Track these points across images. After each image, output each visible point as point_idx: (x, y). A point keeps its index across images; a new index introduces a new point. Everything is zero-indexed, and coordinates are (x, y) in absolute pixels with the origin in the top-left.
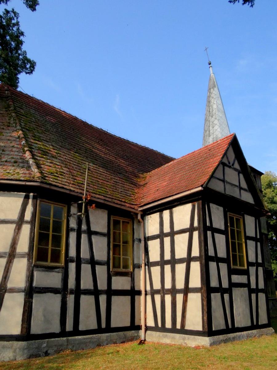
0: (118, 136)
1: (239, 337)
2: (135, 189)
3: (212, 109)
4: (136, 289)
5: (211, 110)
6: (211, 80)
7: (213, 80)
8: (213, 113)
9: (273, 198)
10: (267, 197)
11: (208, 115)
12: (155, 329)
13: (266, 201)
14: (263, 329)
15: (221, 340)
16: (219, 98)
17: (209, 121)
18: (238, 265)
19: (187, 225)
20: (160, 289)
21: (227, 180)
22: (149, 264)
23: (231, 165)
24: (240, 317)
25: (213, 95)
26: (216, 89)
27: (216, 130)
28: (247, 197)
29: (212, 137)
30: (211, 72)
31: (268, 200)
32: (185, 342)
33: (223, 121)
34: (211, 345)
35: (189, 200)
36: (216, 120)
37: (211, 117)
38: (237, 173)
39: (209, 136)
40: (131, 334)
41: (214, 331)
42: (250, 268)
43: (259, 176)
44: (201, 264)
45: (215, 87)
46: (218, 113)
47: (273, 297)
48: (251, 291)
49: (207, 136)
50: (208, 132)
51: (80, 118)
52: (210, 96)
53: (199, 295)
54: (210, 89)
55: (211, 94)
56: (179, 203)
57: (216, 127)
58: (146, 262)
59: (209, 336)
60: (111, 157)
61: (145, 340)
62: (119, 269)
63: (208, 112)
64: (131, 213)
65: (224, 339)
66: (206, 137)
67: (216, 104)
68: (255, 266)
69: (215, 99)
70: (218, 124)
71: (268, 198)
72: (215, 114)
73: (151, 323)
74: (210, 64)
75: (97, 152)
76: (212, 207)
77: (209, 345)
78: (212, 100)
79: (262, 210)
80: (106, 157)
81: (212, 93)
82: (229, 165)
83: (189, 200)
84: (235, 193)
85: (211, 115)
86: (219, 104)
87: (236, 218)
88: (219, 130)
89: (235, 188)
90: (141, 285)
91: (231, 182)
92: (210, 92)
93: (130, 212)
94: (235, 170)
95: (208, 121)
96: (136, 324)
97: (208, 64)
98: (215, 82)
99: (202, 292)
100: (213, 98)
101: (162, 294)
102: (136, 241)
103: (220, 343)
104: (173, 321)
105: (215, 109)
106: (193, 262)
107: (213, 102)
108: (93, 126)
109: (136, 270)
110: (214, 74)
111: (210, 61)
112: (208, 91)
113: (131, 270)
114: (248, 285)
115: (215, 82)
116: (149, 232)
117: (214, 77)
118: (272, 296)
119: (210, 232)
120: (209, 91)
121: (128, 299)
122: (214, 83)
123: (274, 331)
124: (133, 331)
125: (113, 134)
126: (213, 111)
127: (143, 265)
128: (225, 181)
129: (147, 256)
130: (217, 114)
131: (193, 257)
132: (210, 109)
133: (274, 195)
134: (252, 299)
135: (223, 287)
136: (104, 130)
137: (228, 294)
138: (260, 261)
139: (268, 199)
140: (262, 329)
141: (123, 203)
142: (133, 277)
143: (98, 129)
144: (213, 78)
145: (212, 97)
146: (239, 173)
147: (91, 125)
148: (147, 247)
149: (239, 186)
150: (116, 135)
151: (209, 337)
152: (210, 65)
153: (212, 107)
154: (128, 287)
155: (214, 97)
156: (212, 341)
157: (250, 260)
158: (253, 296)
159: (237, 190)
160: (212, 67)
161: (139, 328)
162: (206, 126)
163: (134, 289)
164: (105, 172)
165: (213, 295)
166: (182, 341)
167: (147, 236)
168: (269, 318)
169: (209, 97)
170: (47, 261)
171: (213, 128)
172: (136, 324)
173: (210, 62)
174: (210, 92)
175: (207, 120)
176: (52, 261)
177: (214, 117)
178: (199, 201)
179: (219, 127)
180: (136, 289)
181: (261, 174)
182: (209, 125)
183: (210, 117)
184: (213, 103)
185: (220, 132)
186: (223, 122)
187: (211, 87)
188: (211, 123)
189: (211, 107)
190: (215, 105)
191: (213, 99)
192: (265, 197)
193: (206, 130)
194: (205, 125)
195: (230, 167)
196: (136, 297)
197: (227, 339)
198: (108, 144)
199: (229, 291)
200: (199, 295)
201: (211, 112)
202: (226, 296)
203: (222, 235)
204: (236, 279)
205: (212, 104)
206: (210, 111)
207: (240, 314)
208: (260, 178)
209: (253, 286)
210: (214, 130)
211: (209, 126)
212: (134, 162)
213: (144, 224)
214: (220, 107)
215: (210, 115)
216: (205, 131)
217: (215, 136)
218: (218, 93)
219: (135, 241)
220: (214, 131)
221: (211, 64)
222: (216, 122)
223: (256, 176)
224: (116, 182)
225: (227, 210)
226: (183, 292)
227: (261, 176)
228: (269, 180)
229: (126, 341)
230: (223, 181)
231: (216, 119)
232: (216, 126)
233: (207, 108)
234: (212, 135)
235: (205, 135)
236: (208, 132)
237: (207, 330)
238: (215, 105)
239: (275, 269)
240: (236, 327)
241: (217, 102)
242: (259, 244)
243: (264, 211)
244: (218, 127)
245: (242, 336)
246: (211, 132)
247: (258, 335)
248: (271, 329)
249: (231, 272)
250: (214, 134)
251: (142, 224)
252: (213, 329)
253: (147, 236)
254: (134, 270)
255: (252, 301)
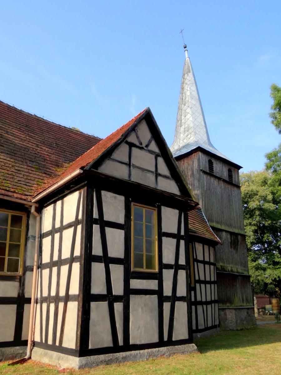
0: (58, 124)
1: (135, 356)
2: (45, 178)
3: (185, 96)
4: (26, 296)
5: (184, 98)
6: (186, 64)
7: (188, 65)
8: (186, 101)
9: (266, 196)
10: (259, 195)
11: (181, 103)
12: (44, 345)
13: (258, 200)
14: (180, 346)
15: (101, 361)
16: (193, 84)
17: (182, 110)
18: (145, 267)
19: (73, 219)
20: (47, 297)
21: (134, 163)
22: (41, 266)
23: (144, 146)
24: (139, 331)
25: (186, 81)
26: (191, 74)
27: (188, 119)
28: (171, 187)
29: (183, 127)
30: (187, 56)
31: (260, 199)
32: (59, 362)
33: (196, 110)
34: (80, 368)
35: (76, 188)
36: (189, 108)
37: (184, 105)
38: (153, 157)
39: (181, 126)
40: (13, 351)
41: (91, 350)
42: (164, 271)
43: (236, 170)
44: (80, 264)
45: (190, 72)
46: (191, 101)
47: (248, 306)
48: (162, 299)
49: (179, 126)
50: (180, 122)
51: (6, 103)
52: (184, 82)
53: (76, 303)
54: (184, 75)
55: (185, 79)
56: (69, 191)
57: (189, 116)
58: (39, 264)
59: (80, 356)
60: (31, 144)
61: (30, 358)
62: (2, 272)
63: (181, 100)
64: (25, 206)
65: (107, 360)
66: (178, 127)
67: (190, 91)
68: (173, 269)
69: (189, 85)
70: (190, 113)
71: (260, 196)
72: (188, 101)
73: (37, 339)
74: (185, 47)
75: (9, 138)
76: (105, 195)
77: (78, 367)
78: (186, 87)
79: (189, 201)
80: (19, 143)
81: (186, 79)
82: (141, 146)
83: (76, 188)
84: (149, 181)
85: (184, 102)
86: (193, 91)
87: (146, 211)
88: (191, 119)
89: (148, 174)
90: (32, 292)
91: (141, 167)
92: (184, 78)
93: (23, 205)
94: (151, 152)
95: (180, 110)
96: (23, 338)
97: (184, 48)
98: (190, 67)
99: (78, 300)
100: (187, 84)
101: (48, 303)
102: (30, 239)
103: (98, 365)
104: (54, 336)
105: (189, 96)
106: (75, 263)
107: (186, 89)
108: (23, 111)
109: (28, 273)
110: (189, 58)
111: (186, 44)
112: (182, 76)
113: (20, 273)
114: (159, 292)
115: (190, 67)
116: (44, 229)
117: (189, 61)
118: (248, 305)
119: (98, 226)
120: (183, 77)
121: (13, 308)
122: (188, 67)
123: (196, 347)
124: (18, 348)
125: (51, 121)
126: (186, 98)
127: (35, 268)
128: (131, 164)
129: (41, 256)
130: (190, 102)
131: (75, 256)
132: (183, 96)
133: (268, 193)
134: (164, 309)
135: (113, 294)
136: (39, 116)
137: (122, 303)
138: (182, 261)
139: (259, 198)
140: (176, 346)
141: (10, 194)
142: (22, 282)
143: (30, 116)
144: (188, 62)
145: (185, 83)
146: (157, 156)
147: (21, 110)
148: (41, 245)
149: (155, 172)
150: (54, 122)
151: (79, 358)
152: (186, 49)
153: (185, 94)
154: (14, 293)
155: (188, 83)
156: (84, 362)
157: (165, 261)
158: (167, 306)
159: (152, 177)
160: (187, 50)
161: (25, 343)
162: (178, 115)
163: (24, 296)
164: (8, 159)
165: (93, 305)
166: (57, 361)
167: (42, 233)
168: (191, 331)
169: (183, 83)
170: (143, 268)
171: (185, 117)
172: (23, 338)
173: (186, 45)
174: (184, 78)
175: (180, 109)
176: (147, 268)
177: (187, 105)
178: (85, 188)
179: (192, 115)
180: (26, 296)
181: (239, 167)
182: (181, 114)
183: (183, 106)
184: (187, 90)
185: (192, 121)
186: (196, 111)
187: (186, 73)
188: (183, 112)
189: (184, 95)
190: (189, 91)
191: (186, 86)
192: (257, 195)
193: (178, 120)
194: (178, 114)
195: (142, 148)
196: (26, 306)
197: (111, 359)
198: (34, 131)
199: (125, 299)
200: (76, 303)
201: (184, 100)
202: (118, 307)
203: (119, 230)
204: (135, 284)
205: (185, 90)
206: (182, 99)
207: (139, 327)
208: (238, 172)
209: (167, 291)
210: (186, 119)
211: (181, 115)
212: (65, 151)
213: (41, 218)
214: (195, 93)
215: (182, 103)
216: (178, 121)
217: (186, 126)
218: (193, 78)
219: (29, 239)
220: (186, 121)
221: (187, 47)
222: (189, 110)
223: (233, 170)
224: (18, 170)
225: (130, 199)
226: (64, 300)
227: (239, 169)
228: (263, 176)
229: (3, 360)
230: (129, 165)
231: (188, 107)
232: (189, 114)
233: (181, 95)
234: (184, 125)
235: (177, 125)
236: (180, 122)
237: (78, 349)
238: (189, 91)
239: (271, 275)
240: (131, 344)
241: (191, 88)
242: (182, 243)
243: (192, 202)
244: (191, 116)
245: (141, 356)
246: (182, 121)
247: (168, 354)
248: (193, 346)
249: (128, 276)
250: (186, 123)
251: (38, 218)
252: (90, 348)
253: (42, 233)
254: (24, 274)
255: (164, 311)
